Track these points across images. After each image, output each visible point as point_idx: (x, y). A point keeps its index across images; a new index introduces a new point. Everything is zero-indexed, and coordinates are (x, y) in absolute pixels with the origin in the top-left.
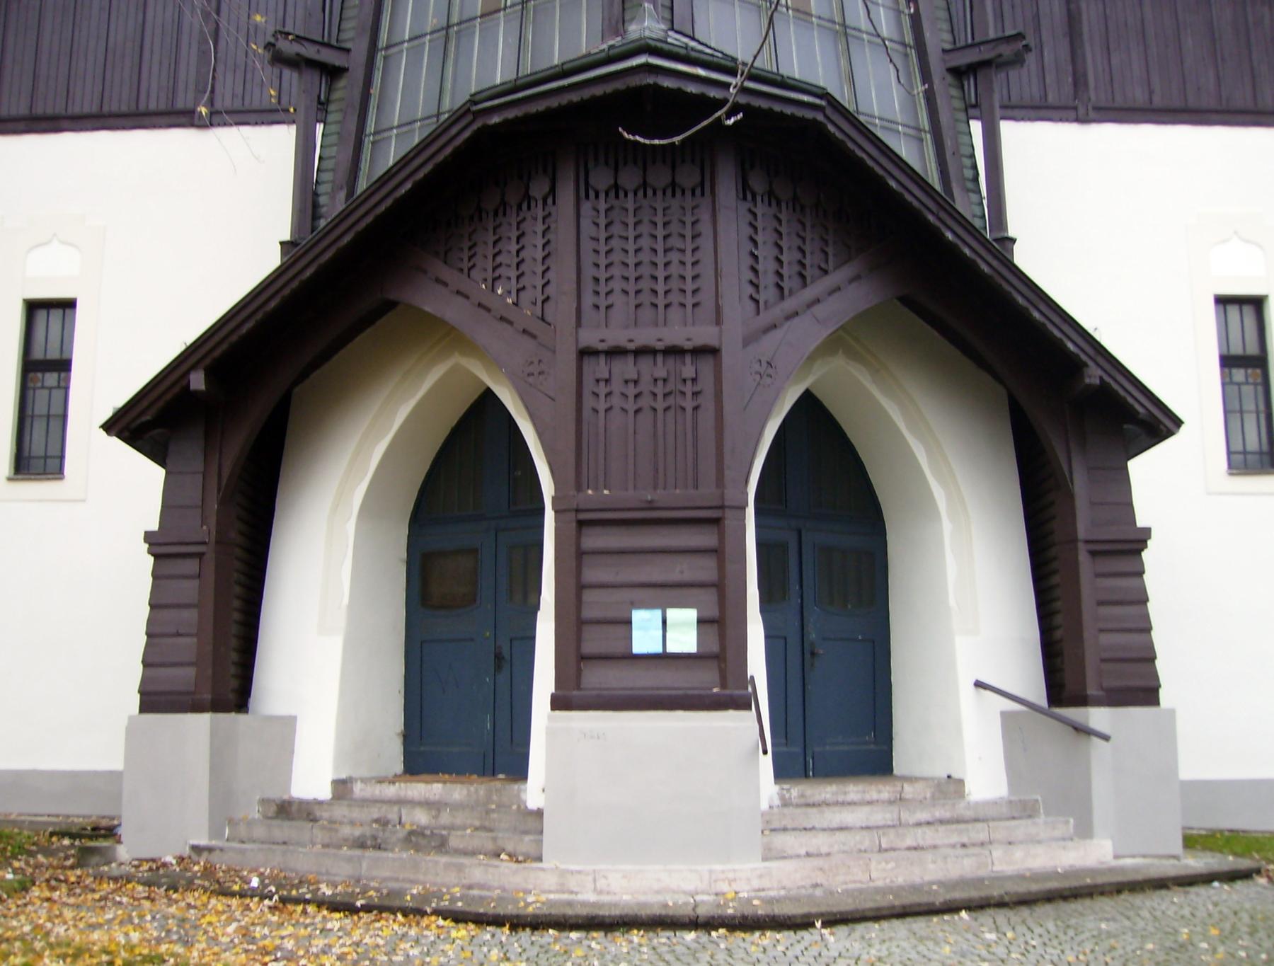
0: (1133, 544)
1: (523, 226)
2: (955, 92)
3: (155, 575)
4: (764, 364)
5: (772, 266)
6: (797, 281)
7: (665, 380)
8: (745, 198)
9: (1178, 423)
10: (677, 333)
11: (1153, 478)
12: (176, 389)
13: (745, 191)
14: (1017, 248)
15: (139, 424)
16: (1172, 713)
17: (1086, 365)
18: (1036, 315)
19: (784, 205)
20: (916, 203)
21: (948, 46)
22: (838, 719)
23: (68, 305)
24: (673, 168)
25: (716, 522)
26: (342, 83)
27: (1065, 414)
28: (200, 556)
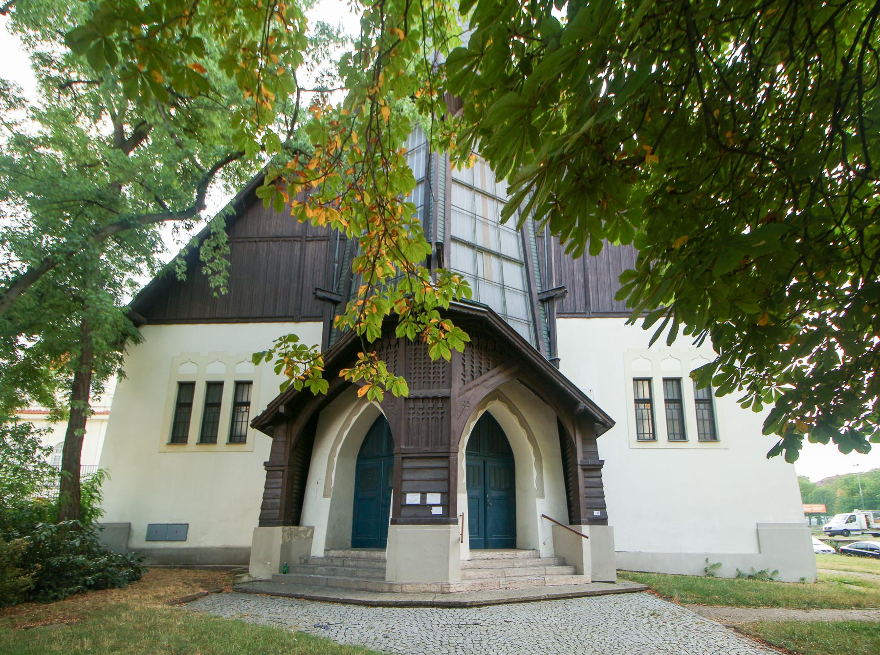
0: (598, 466)
2: (541, 308)
3: (267, 477)
9: (614, 423)
10: (432, 392)
11: (605, 444)
14: (561, 364)
15: (267, 423)
22: (498, 529)
23: (250, 383)
25: (448, 457)
27: (576, 421)
28: (283, 471)
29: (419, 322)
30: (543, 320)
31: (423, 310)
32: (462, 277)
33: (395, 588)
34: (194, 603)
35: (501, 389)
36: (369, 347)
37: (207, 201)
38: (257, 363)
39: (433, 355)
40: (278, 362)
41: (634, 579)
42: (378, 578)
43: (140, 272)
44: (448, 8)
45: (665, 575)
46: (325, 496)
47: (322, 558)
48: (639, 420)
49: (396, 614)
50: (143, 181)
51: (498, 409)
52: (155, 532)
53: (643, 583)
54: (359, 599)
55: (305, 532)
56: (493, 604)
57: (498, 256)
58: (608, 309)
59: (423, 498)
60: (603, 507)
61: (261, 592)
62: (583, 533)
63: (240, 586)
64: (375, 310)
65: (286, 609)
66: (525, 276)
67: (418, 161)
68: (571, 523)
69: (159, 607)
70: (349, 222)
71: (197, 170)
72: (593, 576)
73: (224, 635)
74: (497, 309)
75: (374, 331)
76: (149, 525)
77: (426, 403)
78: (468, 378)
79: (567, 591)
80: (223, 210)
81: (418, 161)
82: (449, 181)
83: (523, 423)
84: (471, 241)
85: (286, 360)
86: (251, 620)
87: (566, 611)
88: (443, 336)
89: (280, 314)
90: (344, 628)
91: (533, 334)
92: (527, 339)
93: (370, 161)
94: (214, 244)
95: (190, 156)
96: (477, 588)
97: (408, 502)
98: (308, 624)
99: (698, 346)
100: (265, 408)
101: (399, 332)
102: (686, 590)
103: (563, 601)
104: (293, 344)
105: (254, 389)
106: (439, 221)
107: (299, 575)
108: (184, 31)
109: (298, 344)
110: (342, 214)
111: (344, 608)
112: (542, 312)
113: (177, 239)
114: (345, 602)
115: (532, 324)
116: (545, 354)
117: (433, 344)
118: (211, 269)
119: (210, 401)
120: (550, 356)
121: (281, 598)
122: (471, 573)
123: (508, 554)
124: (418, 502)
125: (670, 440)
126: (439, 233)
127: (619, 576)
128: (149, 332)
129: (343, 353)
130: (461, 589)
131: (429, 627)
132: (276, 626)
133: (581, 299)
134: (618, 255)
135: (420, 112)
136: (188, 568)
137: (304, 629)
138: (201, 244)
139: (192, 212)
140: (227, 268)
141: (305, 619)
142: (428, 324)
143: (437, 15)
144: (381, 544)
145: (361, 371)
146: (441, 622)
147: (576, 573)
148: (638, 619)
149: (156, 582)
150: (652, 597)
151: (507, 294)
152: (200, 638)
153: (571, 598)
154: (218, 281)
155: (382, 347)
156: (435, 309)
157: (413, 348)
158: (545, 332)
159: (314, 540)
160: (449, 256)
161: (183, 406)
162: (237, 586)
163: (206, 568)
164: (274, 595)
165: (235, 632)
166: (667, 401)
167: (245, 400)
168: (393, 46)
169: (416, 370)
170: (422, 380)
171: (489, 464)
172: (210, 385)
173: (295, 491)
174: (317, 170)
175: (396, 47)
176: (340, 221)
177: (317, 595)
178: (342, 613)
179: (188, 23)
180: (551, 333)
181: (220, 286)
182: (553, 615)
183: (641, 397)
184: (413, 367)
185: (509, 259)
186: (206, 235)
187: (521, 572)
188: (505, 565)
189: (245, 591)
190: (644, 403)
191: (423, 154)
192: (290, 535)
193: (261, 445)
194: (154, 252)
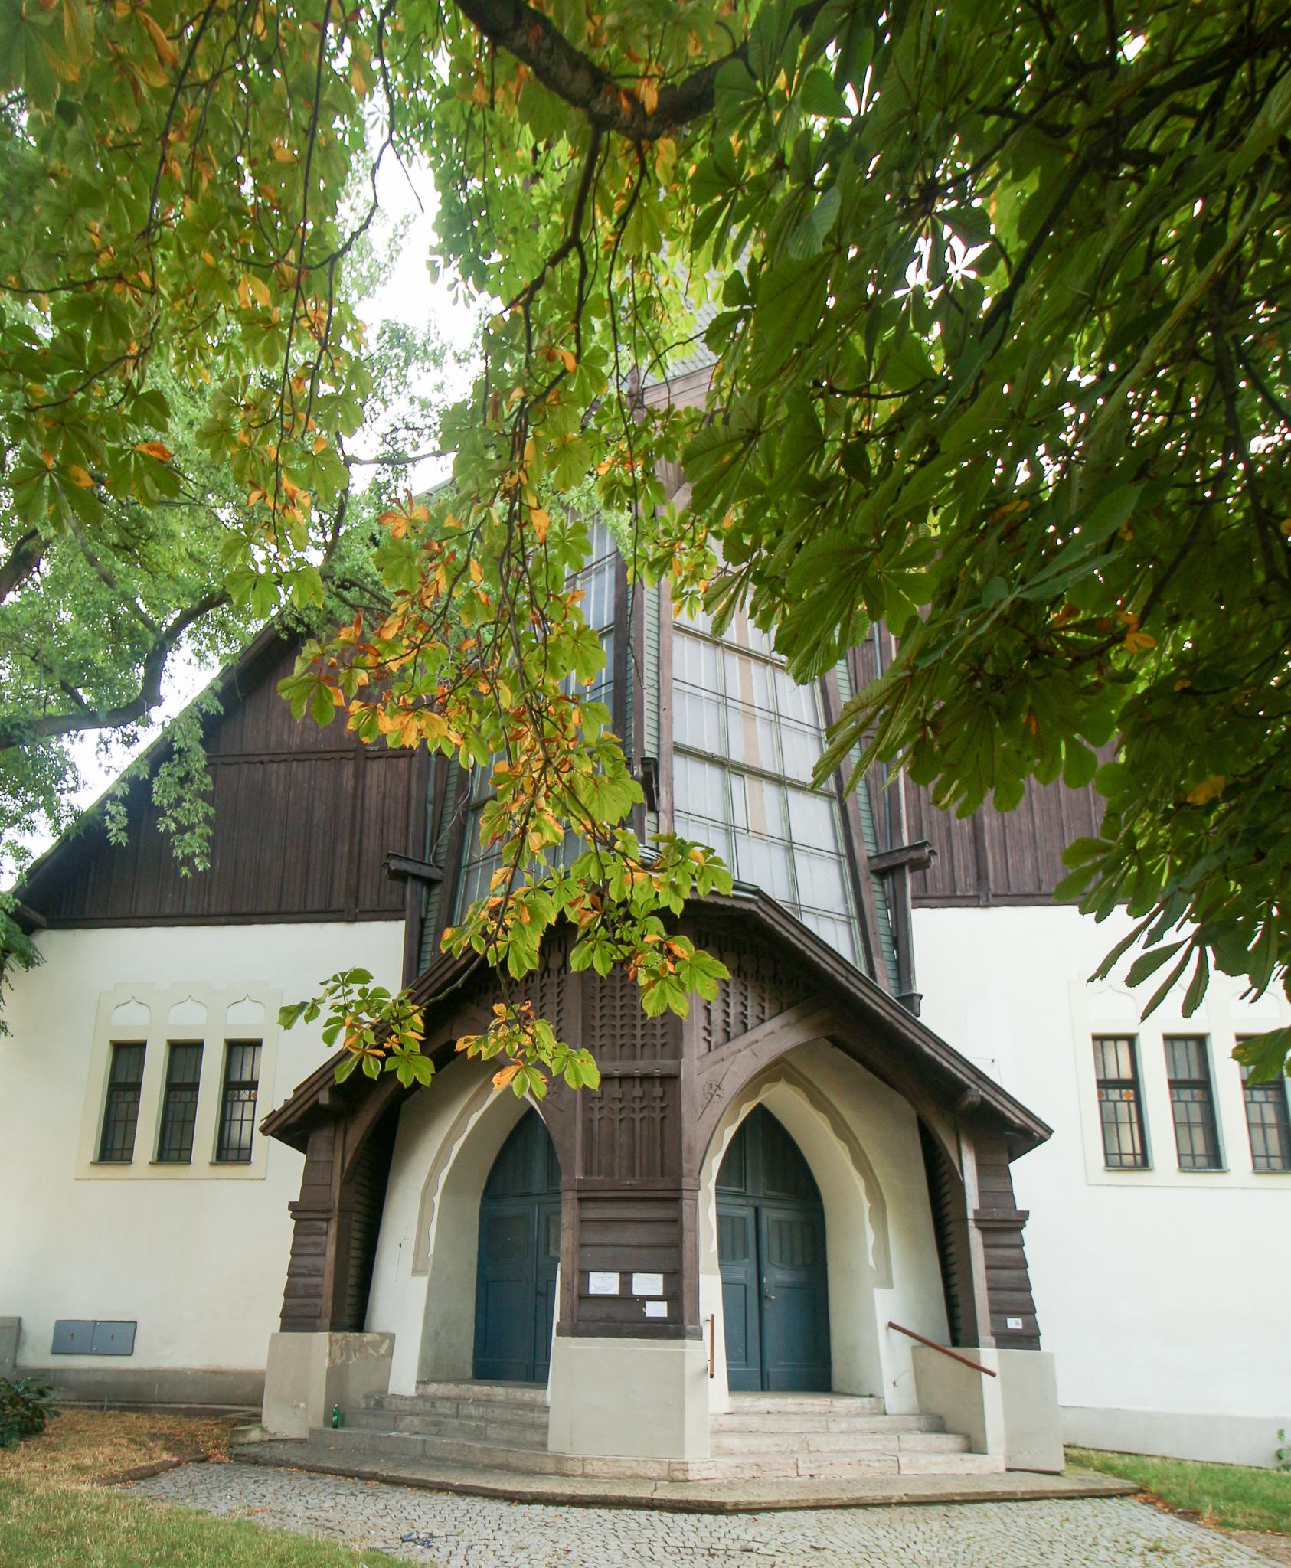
2: (877, 888)
3: (296, 1232)
6: (741, 1027)
9: (1050, 1132)
10: (641, 1066)
11: (1029, 1176)
14: (923, 1004)
15: (295, 1126)
16: (1051, 1356)
17: (969, 1087)
18: (927, 1049)
20: (829, 969)
21: (872, 854)
22: (795, 1348)
23: (257, 1043)
25: (677, 1200)
26: (437, 890)
27: (961, 1123)
29: (621, 941)
30: (881, 913)
31: (628, 916)
32: (711, 851)
33: (568, 1467)
34: (151, 1482)
35: (790, 1058)
36: (516, 990)
37: (165, 689)
38: (288, 1026)
39: (651, 1006)
40: (330, 1022)
41: (1106, 1468)
42: (532, 1445)
43: (31, 827)
44: (662, 280)
45: (1180, 1462)
46: (416, 1272)
47: (412, 1398)
48: (1109, 1124)
49: (572, 1521)
50: (37, 652)
51: (788, 1103)
52: (70, 1336)
53: (1127, 1477)
54: (492, 1486)
55: (376, 1345)
56: (785, 1509)
57: (780, 781)
58: (1029, 888)
59: (626, 1284)
60: (1027, 1310)
61: (288, 1464)
62: (983, 1365)
63: (245, 1450)
64: (526, 918)
65: (341, 1500)
66: (838, 822)
67: (599, 591)
68: (955, 1342)
69: (85, 1488)
70: (464, 737)
71: (141, 626)
72: (1009, 1458)
73: (217, 1553)
74: (778, 891)
75: (523, 953)
76: (61, 1325)
78: (717, 1037)
79: (950, 1488)
80: (197, 704)
81: (599, 591)
82: (667, 631)
83: (842, 1130)
84: (717, 753)
85: (349, 1020)
86: (270, 1521)
87: (950, 1532)
88: (671, 968)
89: (316, 907)
90: (463, 1545)
91: (859, 945)
92: (847, 955)
93: (507, 615)
94: (180, 772)
95: (128, 599)
96: (747, 1475)
97: (593, 1290)
98: (388, 1534)
99: (1254, 1000)
100: (290, 1095)
101: (577, 961)
102: (1232, 1499)
103: (942, 1509)
104: (361, 986)
105: (265, 1053)
106: (646, 713)
107: (366, 1431)
108: (129, 382)
109: (371, 987)
110: (450, 720)
111: (463, 1503)
112: (879, 896)
113: (106, 763)
114: (463, 1492)
115: (856, 922)
116: (885, 984)
117: (651, 985)
118: (175, 820)
119: (177, 1080)
120: (900, 988)
121: (329, 1478)
125: (1182, 1168)
126: (647, 738)
127: (1069, 1459)
128: (51, 943)
129: (455, 995)
130: (712, 1474)
131: (645, 1551)
132: (321, 1536)
133: (966, 869)
134: (1058, 806)
135: (608, 504)
136: (136, 1410)
137: (380, 1545)
138: (154, 772)
139: (135, 710)
140: (207, 820)
141: (383, 1523)
142: (640, 944)
143: (639, 296)
144: (536, 1373)
145: (498, 1041)
146: (671, 1541)
147: (969, 1450)
148: (1120, 1558)
149: (74, 1437)
150: (1149, 1510)
151: (799, 858)
152: (169, 1556)
153: (961, 1502)
154: (192, 846)
156: (653, 913)
158: (885, 939)
160: (670, 785)
161: (122, 1089)
162: (238, 1450)
163: (175, 1412)
164: (316, 1471)
165: (240, 1545)
166: (1175, 1084)
167: (247, 1077)
168: (553, 384)
169: (605, 1021)
171: (767, 1215)
172: (175, 1047)
173: (353, 1262)
174: (398, 638)
175: (558, 387)
176: (444, 734)
177: (404, 1473)
178: (457, 1514)
179: (135, 366)
180: (900, 940)
181: (194, 855)
182: (920, 1538)
183: (1112, 1075)
185: (799, 787)
186: (163, 753)
187: (845, 1443)
189: (255, 1461)
190: (1120, 1089)
192: (346, 1348)
193: (282, 1168)
194: (62, 791)
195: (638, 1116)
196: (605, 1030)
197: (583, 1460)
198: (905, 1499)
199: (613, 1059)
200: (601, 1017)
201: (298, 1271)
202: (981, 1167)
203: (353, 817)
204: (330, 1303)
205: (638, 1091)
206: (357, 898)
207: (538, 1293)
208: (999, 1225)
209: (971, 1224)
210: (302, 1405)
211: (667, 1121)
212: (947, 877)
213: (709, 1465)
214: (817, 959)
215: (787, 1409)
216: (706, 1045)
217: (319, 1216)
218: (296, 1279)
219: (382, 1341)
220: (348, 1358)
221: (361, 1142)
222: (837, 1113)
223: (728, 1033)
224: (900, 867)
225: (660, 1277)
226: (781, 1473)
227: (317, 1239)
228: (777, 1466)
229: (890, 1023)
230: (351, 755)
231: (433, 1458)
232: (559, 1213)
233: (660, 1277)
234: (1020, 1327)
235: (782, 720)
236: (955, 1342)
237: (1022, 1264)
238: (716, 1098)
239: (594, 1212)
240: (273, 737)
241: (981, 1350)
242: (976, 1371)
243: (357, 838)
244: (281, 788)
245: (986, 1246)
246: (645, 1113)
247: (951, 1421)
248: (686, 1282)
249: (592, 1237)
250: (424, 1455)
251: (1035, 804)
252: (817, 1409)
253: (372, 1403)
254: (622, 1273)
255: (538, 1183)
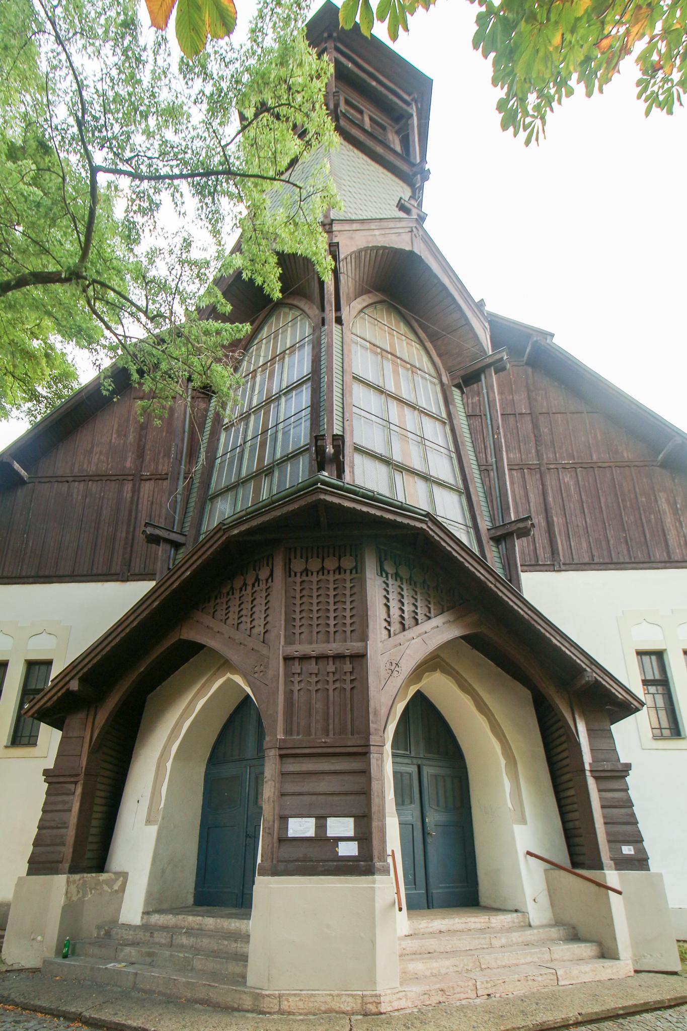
1: (255, 595)
2: (494, 549)
4: (394, 665)
5: (398, 613)
6: (413, 622)
7: (334, 673)
8: (382, 575)
10: (334, 647)
12: (64, 690)
13: (382, 571)
16: (660, 875)
19: (404, 581)
20: (482, 577)
22: (454, 879)
24: (340, 559)
33: (265, 1005)
35: (444, 655)
46: (149, 822)
47: (136, 927)
51: (442, 690)
55: (110, 883)
59: (321, 827)
60: (637, 839)
62: (609, 884)
72: (636, 961)
77: (322, 663)
89: (100, 572)
96: (433, 1001)
97: (291, 833)
106: (335, 412)
112: (496, 554)
122: (418, 967)
123: (473, 921)
124: (311, 833)
130: (403, 1004)
133: (544, 548)
144: (242, 902)
155: (245, 584)
157: (298, 579)
159: (126, 895)
170: (315, 630)
171: (427, 771)
184: (298, 610)
185: (441, 484)
187: (508, 958)
188: (475, 943)
191: (307, 351)
192: (83, 888)
195: (331, 687)
196: (303, 621)
197: (280, 996)
198: (580, 1018)
199: (311, 643)
200: (301, 612)
201: (47, 824)
202: (589, 731)
203: (130, 515)
204: (71, 850)
205: (331, 668)
206: (129, 566)
207: (247, 835)
208: (609, 774)
209: (588, 774)
210: (39, 938)
211: (355, 691)
212: (532, 553)
213: (400, 995)
214: (473, 570)
215: (455, 928)
216: (386, 632)
217: (68, 779)
218: (44, 831)
219: (117, 879)
220: (84, 896)
221: (106, 721)
222: (478, 695)
223: (403, 625)
224: (510, 534)
225: (351, 820)
226: (462, 996)
227: (66, 798)
228: (458, 990)
229: (528, 621)
230: (130, 478)
231: (142, 990)
232: (263, 773)
233: (351, 820)
234: (632, 852)
235: (427, 443)
236: (575, 864)
237: (629, 804)
238: (395, 673)
239: (293, 766)
240: (77, 467)
241: (606, 872)
242: (603, 889)
243: (132, 529)
244: (80, 497)
245: (599, 791)
246: (337, 685)
247: (588, 932)
248: (375, 824)
249: (290, 788)
250: (134, 988)
251: (586, 511)
252: (479, 926)
253: (102, 933)
254: (317, 818)
255: (250, 751)
